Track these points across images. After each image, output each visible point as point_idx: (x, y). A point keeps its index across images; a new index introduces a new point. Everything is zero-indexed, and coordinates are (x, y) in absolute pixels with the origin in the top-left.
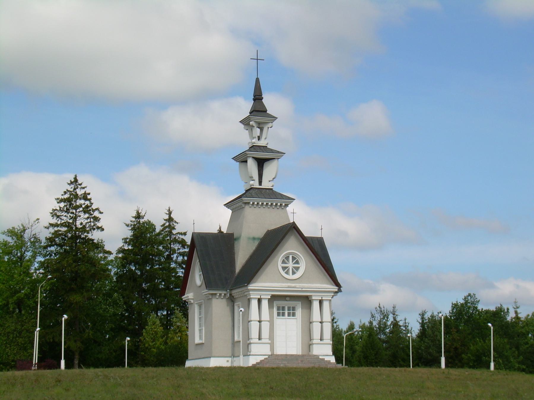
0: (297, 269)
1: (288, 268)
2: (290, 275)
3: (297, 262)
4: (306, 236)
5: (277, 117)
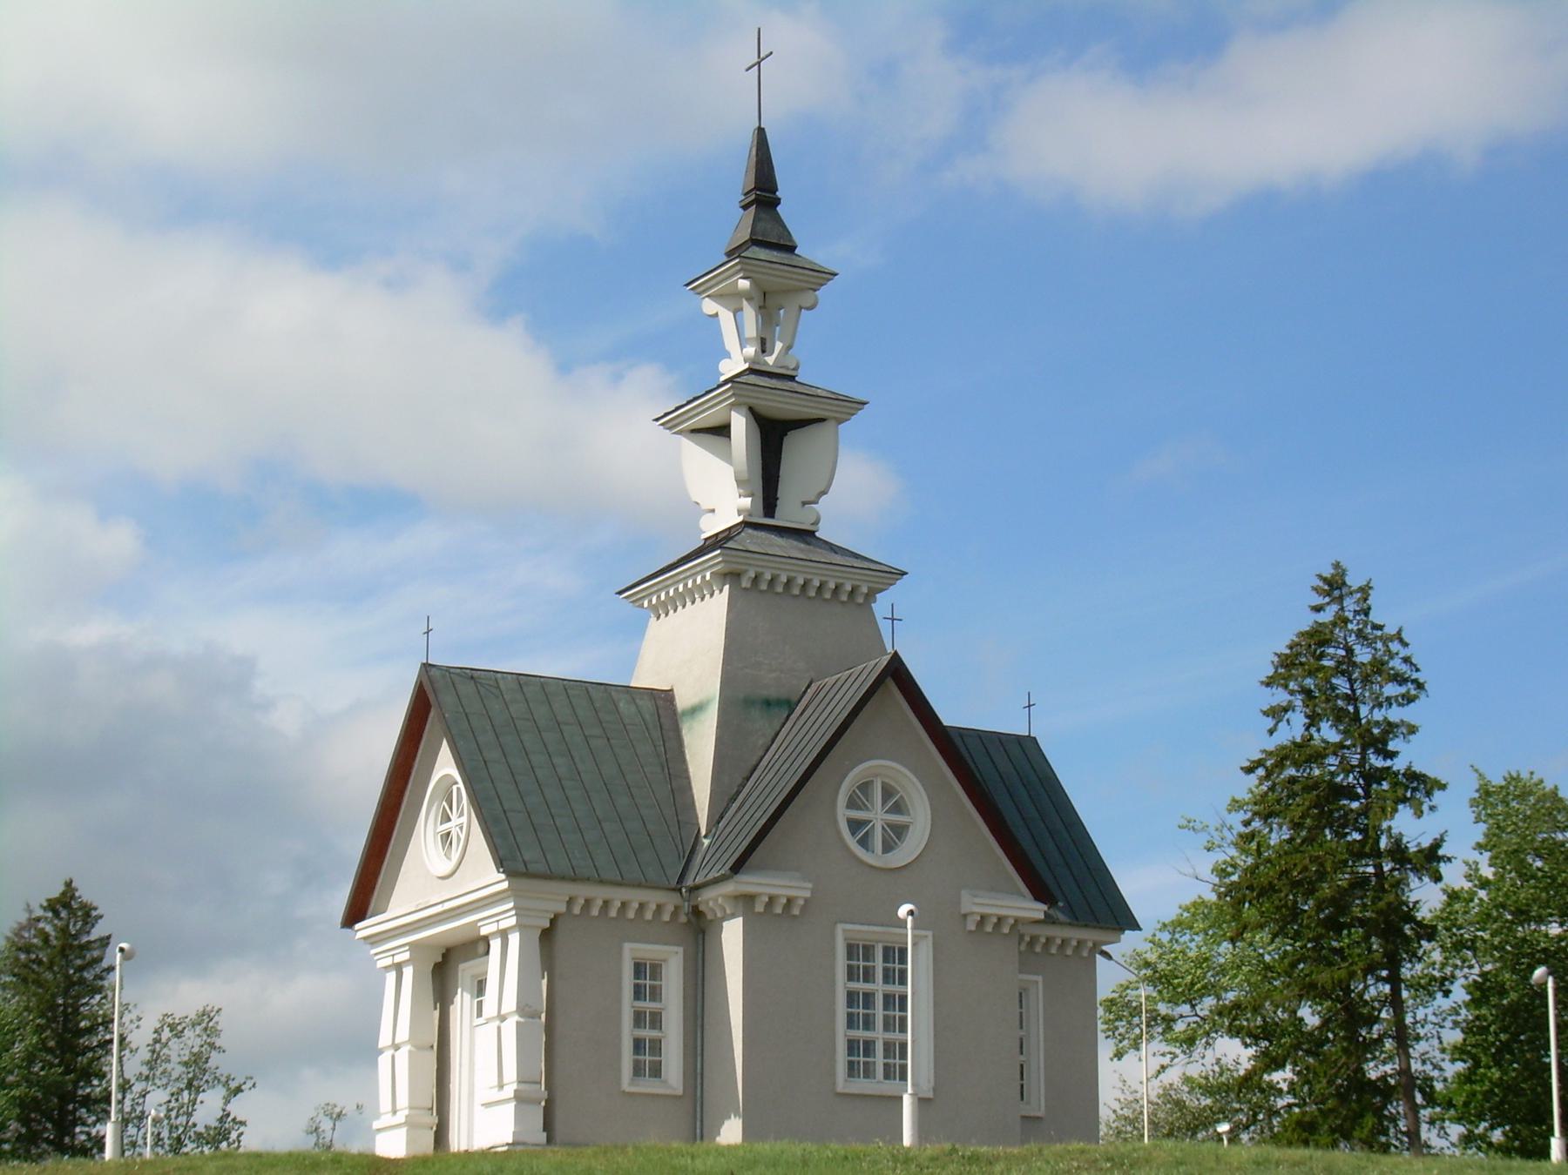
0: (899, 831)
1: (871, 824)
2: (873, 852)
3: (898, 808)
4: (946, 722)
5: (836, 271)
